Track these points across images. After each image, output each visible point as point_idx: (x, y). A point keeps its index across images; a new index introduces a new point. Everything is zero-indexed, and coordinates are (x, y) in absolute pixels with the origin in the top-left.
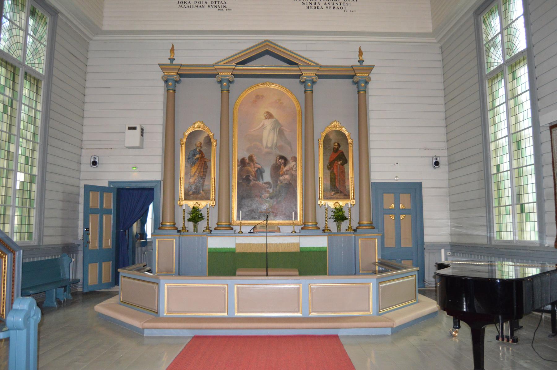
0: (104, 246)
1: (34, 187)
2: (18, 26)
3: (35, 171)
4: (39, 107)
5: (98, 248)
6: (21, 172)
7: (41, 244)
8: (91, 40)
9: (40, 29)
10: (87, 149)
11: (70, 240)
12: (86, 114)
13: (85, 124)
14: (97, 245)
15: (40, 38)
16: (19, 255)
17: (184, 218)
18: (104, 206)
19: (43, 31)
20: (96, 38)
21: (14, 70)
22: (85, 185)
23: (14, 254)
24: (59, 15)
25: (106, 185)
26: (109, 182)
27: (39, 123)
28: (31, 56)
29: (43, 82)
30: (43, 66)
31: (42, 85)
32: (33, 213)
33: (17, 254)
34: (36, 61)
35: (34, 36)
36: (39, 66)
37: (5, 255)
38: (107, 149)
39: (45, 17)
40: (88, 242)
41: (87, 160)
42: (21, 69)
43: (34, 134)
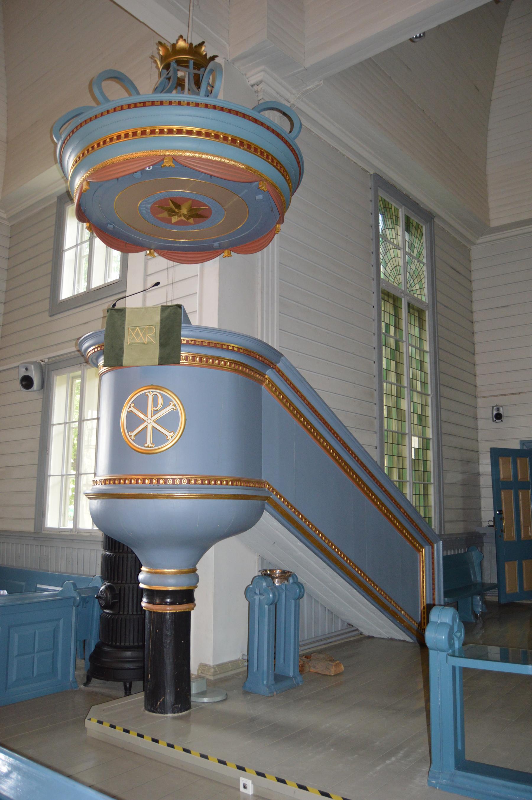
0: (523, 536)
1: (430, 455)
2: (390, 242)
3: (429, 433)
4: (427, 347)
5: (515, 539)
6: (415, 435)
7: (443, 533)
8: (475, 244)
9: (416, 243)
10: (484, 397)
11: (475, 529)
12: (478, 348)
13: (477, 362)
14: (514, 535)
15: (418, 255)
16: (438, 546)
17: (77, 490)
18: (519, 477)
19: (421, 246)
20: (479, 241)
21: (394, 301)
22: (491, 449)
23: (433, 548)
24: (436, 220)
25: (517, 446)
26: (521, 441)
27: (428, 367)
28: (412, 281)
29: (427, 312)
30: (426, 291)
31: (427, 316)
32: (431, 490)
33: (435, 545)
34: (417, 287)
35: (412, 253)
36: (423, 296)
37: (422, 547)
38: (513, 394)
39: (420, 227)
40: (502, 531)
41: (485, 413)
42: (403, 299)
43: (424, 384)
